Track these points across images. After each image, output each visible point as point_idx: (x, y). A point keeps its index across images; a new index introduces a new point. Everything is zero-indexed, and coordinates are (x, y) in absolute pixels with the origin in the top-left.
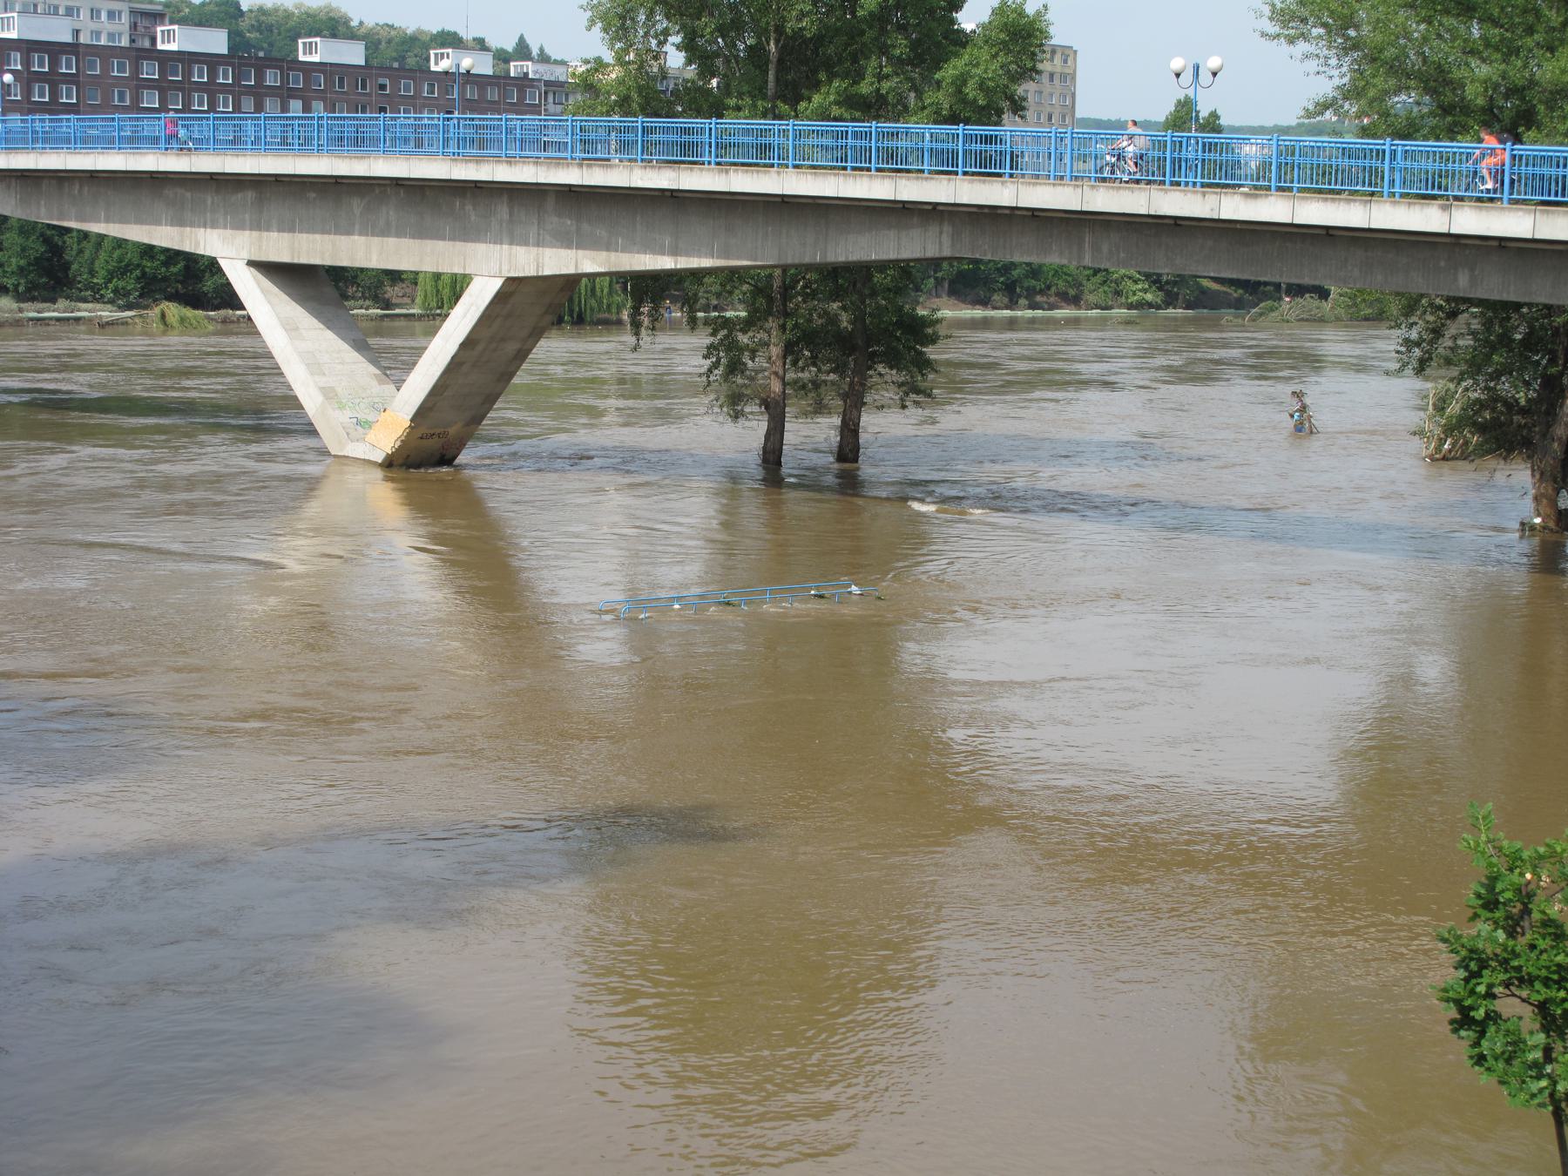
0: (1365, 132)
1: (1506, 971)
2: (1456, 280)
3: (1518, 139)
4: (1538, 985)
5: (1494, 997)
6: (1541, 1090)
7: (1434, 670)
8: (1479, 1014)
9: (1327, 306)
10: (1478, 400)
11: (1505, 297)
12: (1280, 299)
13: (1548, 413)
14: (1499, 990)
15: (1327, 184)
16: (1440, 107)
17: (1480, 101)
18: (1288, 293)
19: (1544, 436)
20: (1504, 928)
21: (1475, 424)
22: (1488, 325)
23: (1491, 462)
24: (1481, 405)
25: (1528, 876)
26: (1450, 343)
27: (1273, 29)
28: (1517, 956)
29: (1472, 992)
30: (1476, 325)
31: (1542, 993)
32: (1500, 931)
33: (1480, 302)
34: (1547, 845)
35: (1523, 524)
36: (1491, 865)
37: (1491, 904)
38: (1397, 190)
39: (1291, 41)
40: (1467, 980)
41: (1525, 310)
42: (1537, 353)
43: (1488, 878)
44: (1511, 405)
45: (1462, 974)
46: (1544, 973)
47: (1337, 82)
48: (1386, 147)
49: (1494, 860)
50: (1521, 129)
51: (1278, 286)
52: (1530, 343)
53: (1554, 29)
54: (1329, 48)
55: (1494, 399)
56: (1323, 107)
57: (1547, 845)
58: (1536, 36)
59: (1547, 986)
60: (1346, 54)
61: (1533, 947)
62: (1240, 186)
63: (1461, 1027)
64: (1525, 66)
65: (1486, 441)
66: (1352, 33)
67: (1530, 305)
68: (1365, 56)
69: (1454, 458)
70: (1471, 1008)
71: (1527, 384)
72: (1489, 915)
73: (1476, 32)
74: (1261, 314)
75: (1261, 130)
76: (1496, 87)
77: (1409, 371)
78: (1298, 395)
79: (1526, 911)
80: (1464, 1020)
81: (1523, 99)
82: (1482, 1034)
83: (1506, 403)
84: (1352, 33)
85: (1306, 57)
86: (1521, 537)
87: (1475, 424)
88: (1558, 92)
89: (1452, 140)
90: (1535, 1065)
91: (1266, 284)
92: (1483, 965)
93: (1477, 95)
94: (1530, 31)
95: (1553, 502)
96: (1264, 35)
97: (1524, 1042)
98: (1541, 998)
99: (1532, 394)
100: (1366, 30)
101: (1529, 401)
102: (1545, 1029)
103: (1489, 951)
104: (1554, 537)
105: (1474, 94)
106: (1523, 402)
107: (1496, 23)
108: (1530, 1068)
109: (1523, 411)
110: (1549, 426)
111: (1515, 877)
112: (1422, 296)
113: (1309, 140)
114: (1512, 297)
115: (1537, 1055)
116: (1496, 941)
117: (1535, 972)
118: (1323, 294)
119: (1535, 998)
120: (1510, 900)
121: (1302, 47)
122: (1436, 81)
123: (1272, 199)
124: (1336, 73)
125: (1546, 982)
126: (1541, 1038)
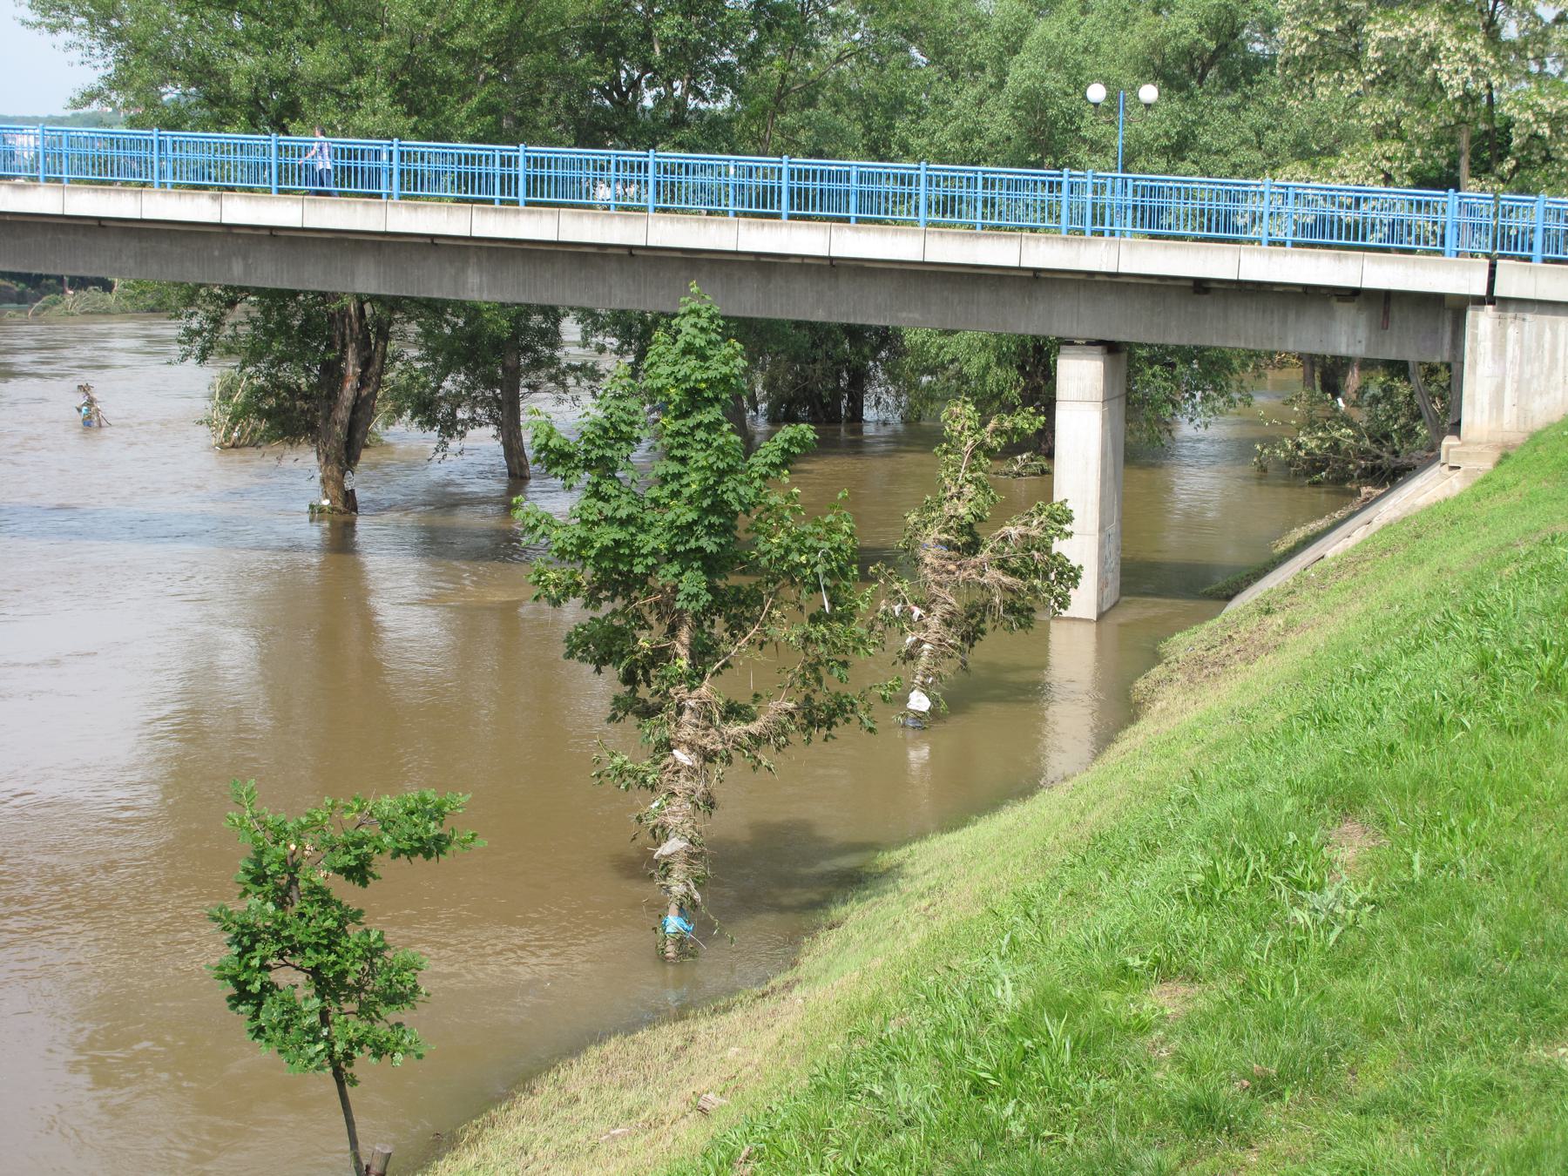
0: (133, 122)
1: (278, 941)
2: (230, 268)
3: (284, 130)
4: (309, 952)
5: (269, 968)
6: (318, 1054)
7: (237, 652)
8: (255, 988)
9: (111, 298)
10: (262, 388)
11: (279, 285)
12: (63, 292)
13: (329, 397)
14: (272, 962)
15: (102, 175)
16: (206, 98)
17: (245, 93)
18: (71, 286)
19: (327, 419)
20: (274, 901)
21: (259, 410)
22: (266, 312)
23: (277, 446)
24: (260, 393)
25: (293, 847)
26: (229, 332)
27: (34, 17)
28: (285, 925)
29: (247, 966)
30: (256, 313)
31: (312, 959)
32: (269, 904)
33: (258, 291)
34: (309, 815)
35: (312, 507)
36: (256, 840)
37: (259, 879)
38: (169, 180)
39: (53, 29)
40: (241, 956)
41: (301, 298)
42: (315, 338)
43: (256, 853)
44: (294, 392)
45: (236, 949)
46: (314, 939)
47: (102, 72)
48: (154, 138)
49: (260, 835)
50: (286, 121)
51: (60, 279)
52: (307, 330)
53: (313, 23)
54: (93, 37)
55: (278, 385)
56: (90, 97)
57: (309, 815)
58: (296, 30)
59: (317, 952)
60: (110, 45)
61: (302, 915)
62: (15, 177)
63: (240, 1002)
64: (287, 59)
65: (272, 428)
66: (115, 23)
67: (306, 293)
68: (129, 47)
69: (243, 446)
70: (247, 982)
71: (307, 370)
72: (259, 889)
73: (238, 25)
74: (45, 309)
75: (34, 121)
76: (260, 78)
77: (192, 361)
78: (84, 389)
79: (294, 881)
80: (242, 995)
81: (286, 91)
82: (260, 1005)
83: (288, 389)
84: (115, 23)
85: (70, 46)
86: (311, 520)
87: (259, 410)
88: (320, 85)
89: (219, 131)
90: (312, 1029)
91: (48, 277)
92: (255, 938)
93: (241, 86)
94: (290, 24)
95: (340, 484)
96: (24, 23)
97: (300, 1009)
98: (313, 964)
99: (313, 380)
100: (128, 19)
101: (310, 386)
102: (320, 993)
103: (260, 924)
104: (342, 518)
105: (238, 85)
106: (304, 388)
107: (256, 16)
108: (307, 1033)
109: (306, 397)
110: (331, 410)
111: (280, 850)
112: (201, 286)
113: (84, 131)
114: (286, 285)
115: (314, 1019)
116: (264, 914)
117: (306, 940)
118: (107, 286)
119: (308, 964)
120: (277, 872)
121: (65, 36)
122: (201, 72)
123: (41, 190)
124: (100, 62)
125: (317, 948)
126: (316, 1002)
